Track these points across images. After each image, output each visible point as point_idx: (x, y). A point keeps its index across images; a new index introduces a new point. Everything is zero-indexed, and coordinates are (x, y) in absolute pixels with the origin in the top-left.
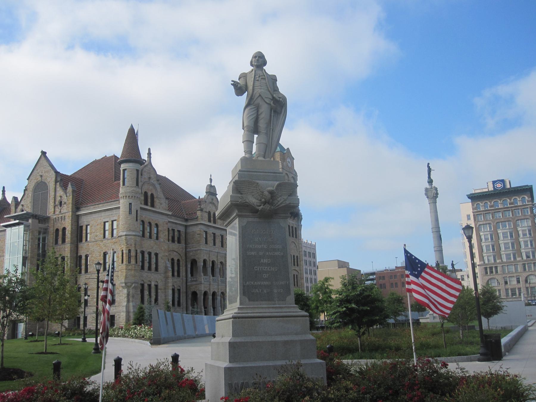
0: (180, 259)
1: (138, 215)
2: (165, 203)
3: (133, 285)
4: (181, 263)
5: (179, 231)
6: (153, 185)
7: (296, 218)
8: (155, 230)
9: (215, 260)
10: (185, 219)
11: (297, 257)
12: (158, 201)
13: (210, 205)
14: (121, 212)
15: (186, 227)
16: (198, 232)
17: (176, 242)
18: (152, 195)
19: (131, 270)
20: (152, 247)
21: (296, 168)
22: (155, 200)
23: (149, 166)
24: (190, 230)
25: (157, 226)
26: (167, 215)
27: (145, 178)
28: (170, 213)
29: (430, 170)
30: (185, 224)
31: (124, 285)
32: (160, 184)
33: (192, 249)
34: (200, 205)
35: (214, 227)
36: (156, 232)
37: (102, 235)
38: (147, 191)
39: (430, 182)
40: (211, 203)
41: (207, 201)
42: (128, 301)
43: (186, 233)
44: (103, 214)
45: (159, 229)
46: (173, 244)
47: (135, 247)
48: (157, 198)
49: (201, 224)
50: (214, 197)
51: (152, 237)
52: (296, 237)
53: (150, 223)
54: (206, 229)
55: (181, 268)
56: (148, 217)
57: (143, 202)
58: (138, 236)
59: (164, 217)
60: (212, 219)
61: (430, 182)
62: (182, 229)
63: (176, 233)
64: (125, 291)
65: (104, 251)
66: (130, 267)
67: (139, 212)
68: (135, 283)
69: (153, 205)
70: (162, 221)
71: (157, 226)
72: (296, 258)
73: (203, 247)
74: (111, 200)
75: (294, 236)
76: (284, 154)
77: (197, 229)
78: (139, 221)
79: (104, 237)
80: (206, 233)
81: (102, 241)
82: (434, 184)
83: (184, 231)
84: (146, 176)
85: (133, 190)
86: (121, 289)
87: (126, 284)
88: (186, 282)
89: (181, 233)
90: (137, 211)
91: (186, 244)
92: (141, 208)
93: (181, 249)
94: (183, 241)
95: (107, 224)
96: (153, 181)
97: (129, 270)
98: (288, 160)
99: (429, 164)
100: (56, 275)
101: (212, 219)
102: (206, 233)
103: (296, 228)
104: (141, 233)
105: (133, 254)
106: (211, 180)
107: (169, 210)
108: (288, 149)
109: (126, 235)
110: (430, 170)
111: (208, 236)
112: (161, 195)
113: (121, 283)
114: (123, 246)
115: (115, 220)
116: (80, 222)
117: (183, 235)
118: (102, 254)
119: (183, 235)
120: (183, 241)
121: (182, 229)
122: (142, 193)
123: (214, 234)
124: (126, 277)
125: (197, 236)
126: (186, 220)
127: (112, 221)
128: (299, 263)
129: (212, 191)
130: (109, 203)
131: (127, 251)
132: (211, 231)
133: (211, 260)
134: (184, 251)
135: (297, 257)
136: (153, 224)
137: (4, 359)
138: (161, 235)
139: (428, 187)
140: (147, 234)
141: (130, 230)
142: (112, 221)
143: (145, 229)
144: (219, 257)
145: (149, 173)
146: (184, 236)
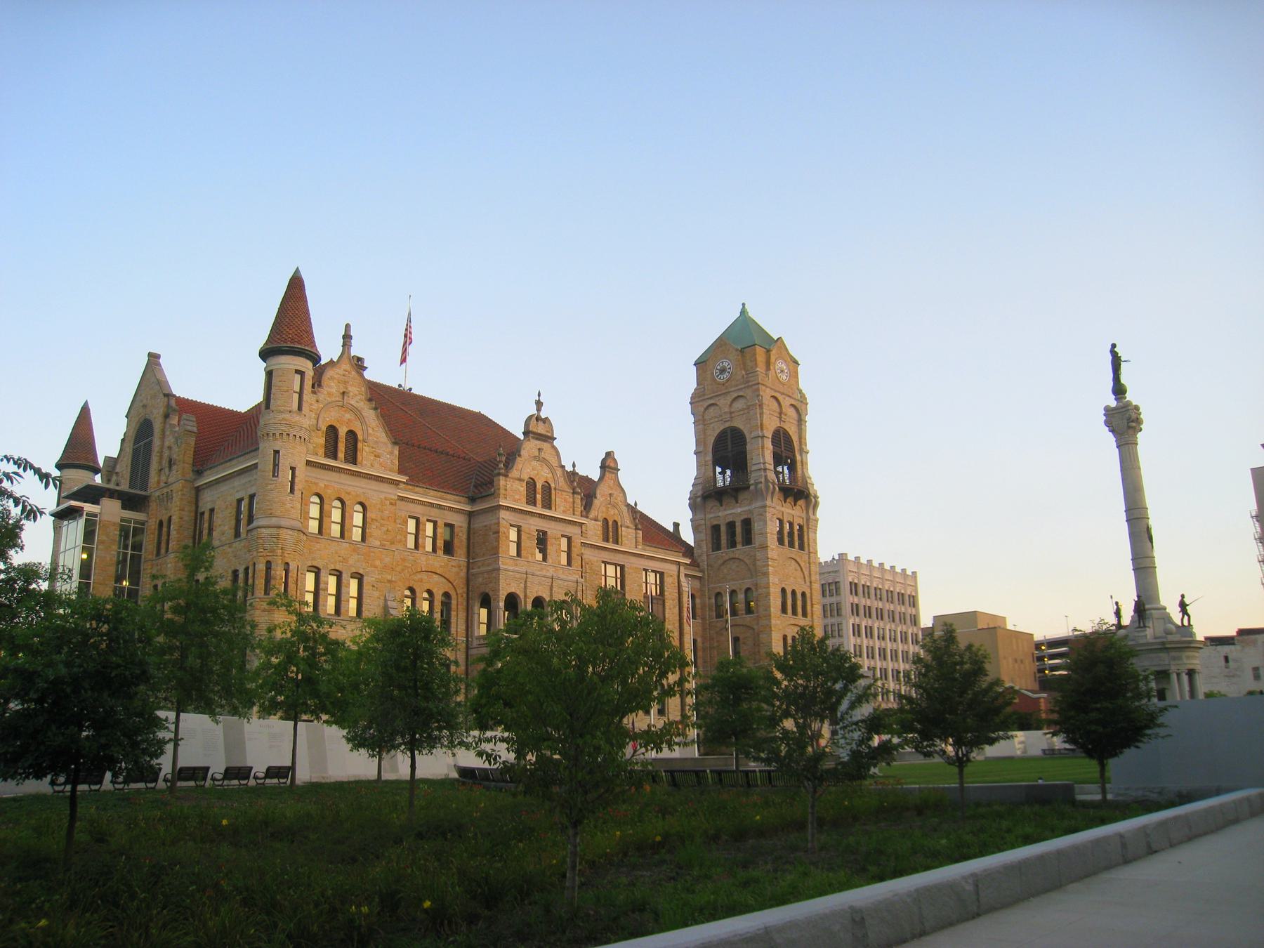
0: (452, 593)
2: (391, 453)
4: (454, 602)
5: (450, 526)
7: (801, 502)
11: (803, 594)
12: (366, 449)
13: (534, 463)
18: (352, 435)
20: (345, 560)
21: (802, 385)
22: (360, 445)
26: (396, 483)
27: (330, 394)
29: (1116, 362)
30: (468, 508)
33: (482, 569)
35: (541, 516)
37: (232, 532)
38: (337, 425)
39: (1119, 390)
44: (237, 482)
45: (368, 515)
50: (546, 446)
52: (802, 547)
55: (453, 613)
61: (1119, 390)
69: (352, 457)
72: (799, 596)
82: (1129, 396)
83: (465, 525)
88: (467, 648)
89: (456, 530)
91: (468, 556)
92: (309, 463)
93: (454, 570)
94: (460, 550)
98: (780, 364)
99: (1114, 346)
100: (99, 621)
106: (539, 404)
110: (1116, 362)
111: (523, 537)
116: (200, 504)
117: (461, 536)
121: (459, 521)
128: (809, 608)
129: (541, 429)
134: (463, 574)
135: (803, 594)
137: (1097, 775)
138: (372, 529)
139: (1113, 404)
145: (345, 382)
146: (465, 537)
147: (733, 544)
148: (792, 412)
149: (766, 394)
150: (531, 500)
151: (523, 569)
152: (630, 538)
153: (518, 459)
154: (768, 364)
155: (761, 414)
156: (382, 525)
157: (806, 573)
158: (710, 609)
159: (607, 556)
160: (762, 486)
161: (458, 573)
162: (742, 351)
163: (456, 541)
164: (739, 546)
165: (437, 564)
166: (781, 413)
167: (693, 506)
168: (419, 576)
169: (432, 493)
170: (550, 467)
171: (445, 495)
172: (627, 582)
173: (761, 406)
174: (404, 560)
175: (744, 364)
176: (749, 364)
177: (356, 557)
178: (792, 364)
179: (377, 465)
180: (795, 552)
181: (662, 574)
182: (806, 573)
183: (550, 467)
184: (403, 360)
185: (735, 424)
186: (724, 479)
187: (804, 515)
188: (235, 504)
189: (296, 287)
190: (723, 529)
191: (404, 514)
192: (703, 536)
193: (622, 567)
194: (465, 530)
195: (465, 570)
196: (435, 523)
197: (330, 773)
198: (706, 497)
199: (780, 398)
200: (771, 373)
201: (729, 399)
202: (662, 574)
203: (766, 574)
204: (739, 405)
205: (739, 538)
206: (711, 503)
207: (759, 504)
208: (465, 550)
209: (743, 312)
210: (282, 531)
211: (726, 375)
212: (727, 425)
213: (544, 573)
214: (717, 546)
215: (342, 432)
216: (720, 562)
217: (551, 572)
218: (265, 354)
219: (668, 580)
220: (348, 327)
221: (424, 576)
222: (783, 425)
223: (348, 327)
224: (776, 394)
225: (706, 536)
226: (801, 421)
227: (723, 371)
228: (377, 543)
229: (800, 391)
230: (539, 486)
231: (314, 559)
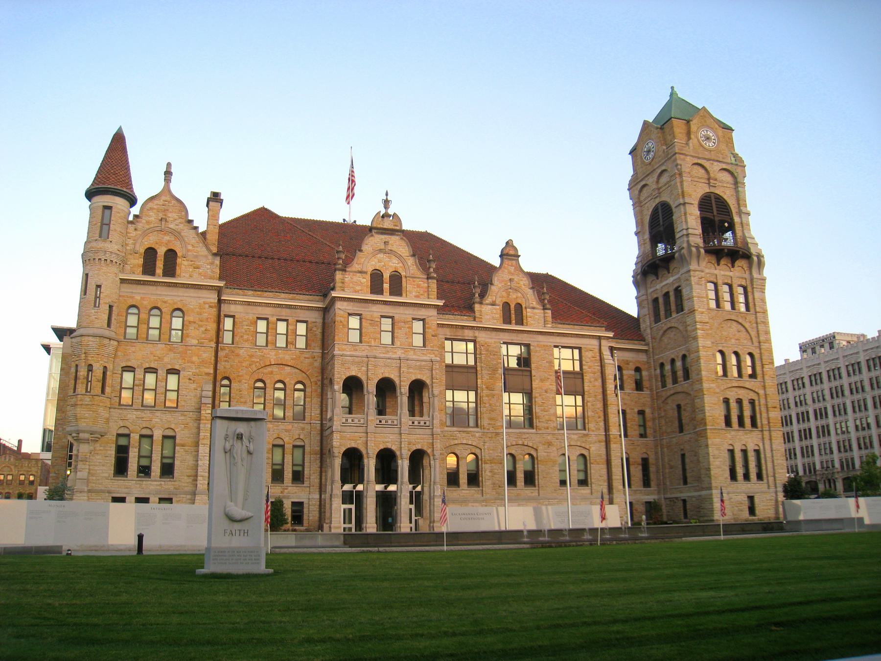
2: (212, 263)
7: (740, 263)
12: (185, 263)
13: (381, 256)
27: (148, 222)
30: (320, 305)
47: (86, 359)
106: (386, 203)
134: (318, 364)
147: (668, 313)
148: (726, 177)
149: (686, 163)
151: (364, 354)
152: (537, 317)
153: (359, 254)
154: (689, 134)
155: (682, 182)
158: (656, 380)
159: (507, 337)
160: (684, 251)
161: (311, 364)
162: (662, 128)
164: (674, 315)
165: (287, 357)
167: (636, 283)
168: (269, 369)
169: (283, 295)
171: (297, 297)
173: (681, 175)
174: (251, 356)
175: (665, 139)
176: (669, 138)
177: (172, 355)
178: (720, 132)
179: (196, 275)
182: (753, 334)
185: (663, 199)
187: (747, 276)
189: (118, 142)
191: (252, 317)
194: (320, 325)
195: (319, 360)
197: (110, 543)
198: (649, 270)
200: (693, 142)
201: (656, 175)
203: (695, 338)
204: (664, 179)
205: (673, 307)
206: (651, 278)
207: (685, 270)
208: (319, 343)
209: (673, 94)
210: (83, 339)
211: (651, 155)
212: (657, 201)
213: (390, 355)
214: (657, 319)
215: (161, 251)
216: (661, 333)
217: (399, 353)
218: (90, 194)
219: (587, 355)
220: (169, 165)
221: (275, 369)
222: (712, 190)
223: (169, 165)
225: (648, 310)
226: (737, 184)
227: (649, 151)
228: (195, 342)
231: (129, 360)
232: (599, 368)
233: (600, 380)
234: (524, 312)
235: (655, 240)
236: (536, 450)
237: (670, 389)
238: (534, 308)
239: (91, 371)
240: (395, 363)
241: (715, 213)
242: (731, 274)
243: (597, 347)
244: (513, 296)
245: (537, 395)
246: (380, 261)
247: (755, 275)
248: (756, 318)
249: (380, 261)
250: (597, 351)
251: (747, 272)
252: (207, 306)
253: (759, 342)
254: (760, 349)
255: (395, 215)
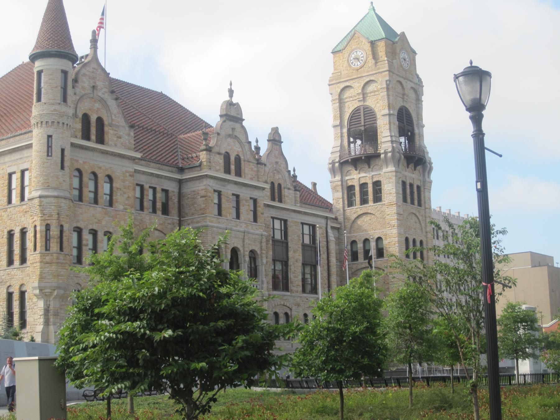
1: (66, 159)
2: (129, 135)
3: (56, 293)
5: (166, 191)
6: (102, 101)
7: (419, 168)
8: (106, 188)
9: (239, 246)
10: (178, 168)
12: (111, 132)
13: (229, 140)
14: (34, 154)
15: (180, 182)
16: (203, 193)
17: (159, 213)
18: (100, 121)
19: (50, 263)
20: (99, 222)
21: (420, 71)
22: (106, 129)
23: (94, 65)
24: (188, 189)
25: (110, 179)
27: (83, 88)
28: (138, 155)
30: (178, 177)
31: (37, 292)
32: (117, 99)
34: (205, 139)
35: (236, 183)
36: (108, 192)
37: (6, 199)
40: (230, 136)
41: (223, 133)
42: (47, 323)
43: (180, 195)
45: (115, 185)
46: (153, 216)
47: (58, 219)
48: (110, 125)
49: (206, 176)
50: (237, 125)
51: (100, 200)
52: (420, 204)
53: (95, 174)
54: (218, 187)
56: (90, 161)
57: (79, 134)
58: (65, 198)
59: (126, 163)
60: (233, 167)
62: (172, 187)
63: (159, 195)
64: (41, 304)
65: (9, 229)
66: (48, 258)
67: (66, 153)
68: (58, 288)
69: (101, 139)
70: (120, 169)
71: (110, 179)
73: (211, 220)
74: (19, 132)
75: (416, 202)
76: (394, 43)
77: (200, 187)
78: (67, 169)
79: (10, 201)
80: (220, 193)
81: (5, 210)
83: (176, 190)
84: (85, 83)
85: (55, 110)
86: (35, 299)
87: (41, 290)
89: (170, 195)
90: (63, 151)
92: (73, 145)
94: (174, 211)
95: (14, 177)
96: (103, 92)
97: (47, 263)
101: (233, 167)
102: (220, 193)
103: (419, 188)
104: (76, 193)
105: (55, 232)
106: (231, 92)
107: (136, 150)
108: (403, 34)
109: (40, 197)
111: (223, 200)
112: (121, 122)
113: (34, 288)
114: (36, 218)
115: (27, 170)
117: (174, 199)
118: (6, 233)
119: (174, 199)
120: (174, 211)
121: (172, 187)
122: (75, 115)
123: (238, 196)
124: (41, 278)
125: (200, 200)
126: (181, 170)
127: (23, 172)
129: (233, 113)
130: (17, 138)
131: (44, 228)
132: (228, 190)
133: (230, 247)
136: (101, 176)
138: (118, 197)
140: (88, 195)
141: (48, 187)
142: (23, 172)
143: (85, 187)
144: (246, 241)
145: (94, 78)
150: (227, 171)
156: (125, 193)
157: (423, 225)
159: (274, 213)
163: (170, 203)
164: (371, 203)
166: (404, 95)
170: (240, 143)
172: (290, 233)
180: (414, 208)
181: (314, 227)
183: (240, 143)
184: (501, 156)
186: (357, 148)
187: (421, 178)
188: (7, 177)
190: (357, 189)
192: (340, 194)
193: (285, 221)
194: (176, 194)
196: (154, 189)
198: (346, 163)
199: (404, 82)
202: (285, 221)
215: (93, 118)
217: (243, 228)
224: (401, 80)
226: (418, 100)
229: (418, 76)
230: (232, 159)
231: (78, 221)
232: (326, 243)
233: (326, 254)
234: (283, 192)
235: (354, 134)
236: (291, 309)
237: (362, 263)
238: (289, 189)
239: (49, 230)
240: (241, 235)
241: (405, 123)
242: (413, 176)
243: (325, 226)
244: (277, 177)
245: (292, 264)
246: (229, 145)
247: (427, 179)
248: (425, 213)
249: (229, 145)
250: (324, 228)
251: (422, 175)
252: (128, 174)
253: (426, 232)
254: (427, 238)
255: (237, 104)
